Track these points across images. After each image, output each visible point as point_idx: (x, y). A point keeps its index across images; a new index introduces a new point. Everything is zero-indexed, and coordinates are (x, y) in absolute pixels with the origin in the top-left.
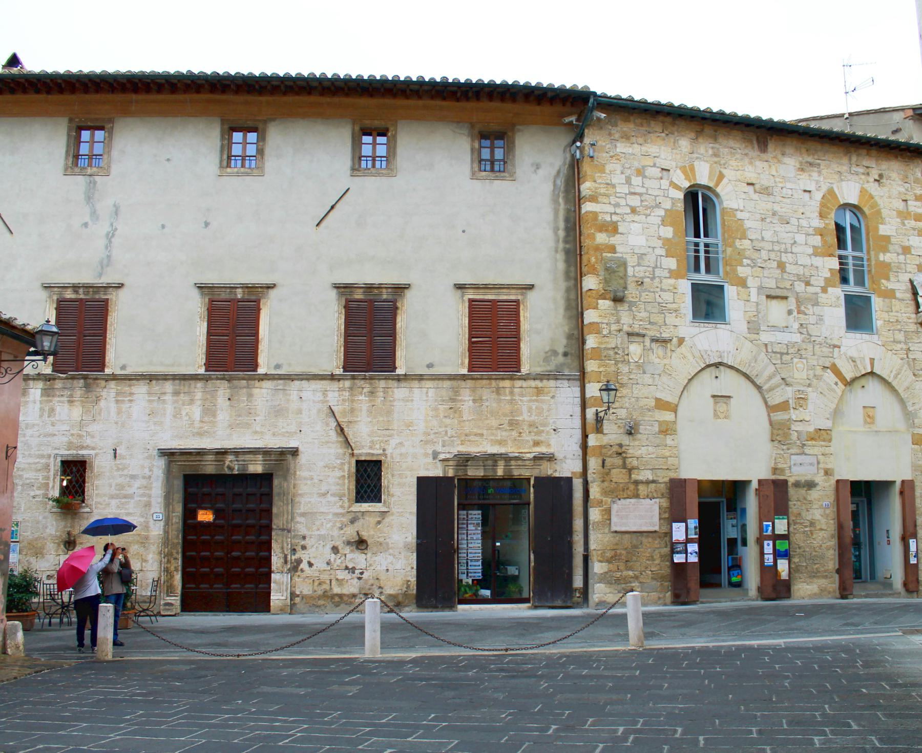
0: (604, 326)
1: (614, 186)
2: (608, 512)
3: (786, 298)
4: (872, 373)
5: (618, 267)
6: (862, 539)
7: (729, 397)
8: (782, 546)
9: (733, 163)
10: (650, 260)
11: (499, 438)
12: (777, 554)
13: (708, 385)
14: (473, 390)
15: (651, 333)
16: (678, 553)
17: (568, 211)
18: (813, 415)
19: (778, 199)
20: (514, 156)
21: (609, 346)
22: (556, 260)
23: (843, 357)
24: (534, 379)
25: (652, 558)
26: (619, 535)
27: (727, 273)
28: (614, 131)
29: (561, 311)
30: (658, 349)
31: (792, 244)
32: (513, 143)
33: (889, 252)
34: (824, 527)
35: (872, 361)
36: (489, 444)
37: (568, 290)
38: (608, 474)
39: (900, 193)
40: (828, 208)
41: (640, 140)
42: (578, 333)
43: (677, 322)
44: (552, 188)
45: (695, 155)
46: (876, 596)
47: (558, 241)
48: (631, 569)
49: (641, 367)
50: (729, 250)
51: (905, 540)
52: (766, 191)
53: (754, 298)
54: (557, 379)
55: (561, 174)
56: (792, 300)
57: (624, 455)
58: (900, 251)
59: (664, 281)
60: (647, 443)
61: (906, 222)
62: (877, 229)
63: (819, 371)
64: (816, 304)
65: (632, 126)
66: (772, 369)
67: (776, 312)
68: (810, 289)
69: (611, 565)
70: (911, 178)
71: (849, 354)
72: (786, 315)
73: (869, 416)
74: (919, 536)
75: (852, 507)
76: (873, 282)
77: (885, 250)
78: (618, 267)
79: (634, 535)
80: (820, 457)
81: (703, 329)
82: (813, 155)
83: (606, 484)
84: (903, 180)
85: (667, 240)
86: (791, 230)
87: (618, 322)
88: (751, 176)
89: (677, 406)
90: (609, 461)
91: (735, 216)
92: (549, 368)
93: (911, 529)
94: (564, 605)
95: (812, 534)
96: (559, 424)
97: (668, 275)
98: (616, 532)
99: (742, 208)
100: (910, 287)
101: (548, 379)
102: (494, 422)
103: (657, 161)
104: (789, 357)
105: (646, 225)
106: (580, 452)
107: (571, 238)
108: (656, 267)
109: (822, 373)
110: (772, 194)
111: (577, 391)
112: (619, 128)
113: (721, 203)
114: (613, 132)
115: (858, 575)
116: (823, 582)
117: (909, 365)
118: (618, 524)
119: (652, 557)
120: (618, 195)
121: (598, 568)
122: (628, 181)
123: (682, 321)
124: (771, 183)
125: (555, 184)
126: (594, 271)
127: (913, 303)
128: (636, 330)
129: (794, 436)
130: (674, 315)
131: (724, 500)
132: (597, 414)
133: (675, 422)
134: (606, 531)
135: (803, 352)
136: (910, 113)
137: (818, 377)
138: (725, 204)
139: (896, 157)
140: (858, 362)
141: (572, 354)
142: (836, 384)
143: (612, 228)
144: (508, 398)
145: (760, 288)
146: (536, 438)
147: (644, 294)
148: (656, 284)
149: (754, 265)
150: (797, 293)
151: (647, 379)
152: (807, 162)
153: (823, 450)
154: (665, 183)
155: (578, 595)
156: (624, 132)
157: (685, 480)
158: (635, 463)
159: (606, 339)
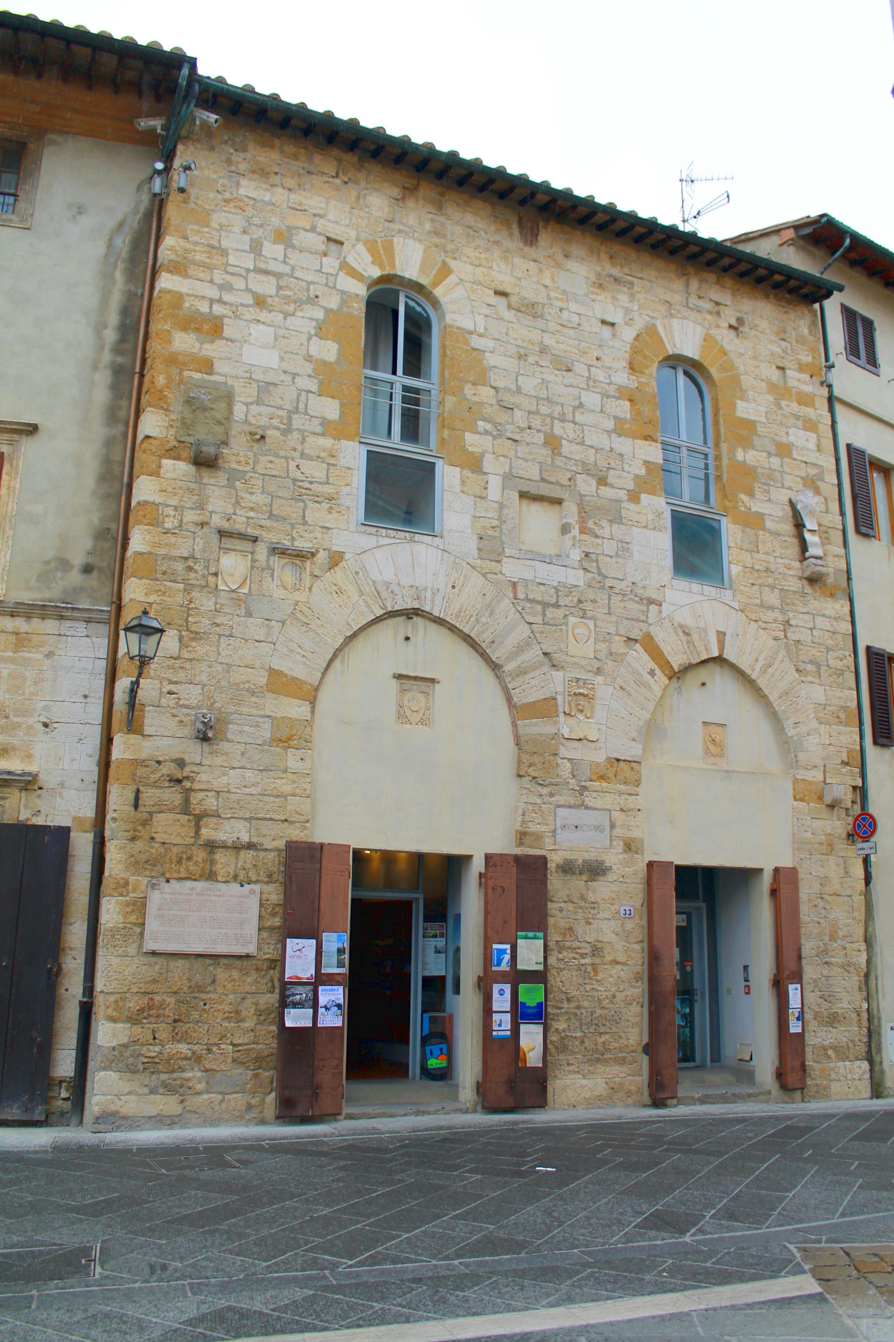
1: (224, 253)
2: (140, 906)
3: (559, 502)
4: (720, 660)
5: (216, 400)
6: (697, 984)
7: (433, 681)
8: (531, 995)
9: (469, 251)
12: (522, 1014)
13: (387, 651)
16: (295, 1005)
17: (130, 297)
18: (603, 729)
19: (552, 326)
21: (176, 553)
23: (667, 623)
25: (236, 1016)
26: (161, 960)
27: (442, 441)
28: (238, 157)
29: (90, 481)
30: (285, 572)
31: (575, 408)
33: (753, 448)
34: (622, 958)
35: (721, 635)
37: (109, 443)
40: (645, 357)
41: (290, 182)
43: (330, 520)
44: (103, 250)
45: (397, 226)
46: (724, 1099)
47: (101, 348)
48: (184, 1038)
49: (243, 603)
50: (450, 401)
51: (779, 985)
52: (530, 310)
53: (494, 491)
54: (62, 618)
55: (126, 229)
56: (571, 507)
58: (773, 450)
59: (311, 439)
60: (244, 762)
61: (783, 403)
62: (733, 406)
63: (619, 645)
64: (617, 519)
65: (275, 155)
66: (523, 632)
67: (538, 526)
68: (605, 491)
69: (137, 1030)
70: (792, 335)
73: (715, 741)
74: (806, 977)
75: (676, 920)
77: (747, 444)
79: (198, 964)
80: (616, 815)
82: (622, 266)
83: (140, 845)
84: (778, 334)
85: (325, 363)
86: (575, 383)
88: (505, 281)
89: (317, 689)
90: (149, 796)
91: (467, 342)
92: (47, 595)
93: (789, 965)
94: (24, 1118)
95: (595, 971)
97: (319, 429)
98: (154, 953)
99: (482, 331)
100: (790, 514)
103: (320, 223)
104: (560, 613)
105: (282, 332)
109: (623, 649)
110: (542, 317)
112: (248, 156)
115: (687, 1054)
116: (617, 1073)
117: (788, 651)
119: (238, 1012)
120: (229, 269)
121: (107, 1034)
122: (256, 248)
123: (342, 522)
124: (541, 298)
125: (110, 245)
126: (162, 403)
127: (795, 541)
131: (420, 896)
133: (309, 723)
134: (132, 950)
135: (588, 606)
137: (617, 658)
138: (449, 318)
139: (767, 296)
140: (695, 637)
141: (101, 570)
142: (652, 673)
143: (213, 329)
145: (508, 478)
147: (263, 460)
148: (292, 444)
149: (498, 433)
150: (581, 496)
151: (254, 628)
152: (610, 276)
153: (622, 800)
154: (331, 263)
155: (64, 1094)
157: (322, 845)
158: (211, 802)
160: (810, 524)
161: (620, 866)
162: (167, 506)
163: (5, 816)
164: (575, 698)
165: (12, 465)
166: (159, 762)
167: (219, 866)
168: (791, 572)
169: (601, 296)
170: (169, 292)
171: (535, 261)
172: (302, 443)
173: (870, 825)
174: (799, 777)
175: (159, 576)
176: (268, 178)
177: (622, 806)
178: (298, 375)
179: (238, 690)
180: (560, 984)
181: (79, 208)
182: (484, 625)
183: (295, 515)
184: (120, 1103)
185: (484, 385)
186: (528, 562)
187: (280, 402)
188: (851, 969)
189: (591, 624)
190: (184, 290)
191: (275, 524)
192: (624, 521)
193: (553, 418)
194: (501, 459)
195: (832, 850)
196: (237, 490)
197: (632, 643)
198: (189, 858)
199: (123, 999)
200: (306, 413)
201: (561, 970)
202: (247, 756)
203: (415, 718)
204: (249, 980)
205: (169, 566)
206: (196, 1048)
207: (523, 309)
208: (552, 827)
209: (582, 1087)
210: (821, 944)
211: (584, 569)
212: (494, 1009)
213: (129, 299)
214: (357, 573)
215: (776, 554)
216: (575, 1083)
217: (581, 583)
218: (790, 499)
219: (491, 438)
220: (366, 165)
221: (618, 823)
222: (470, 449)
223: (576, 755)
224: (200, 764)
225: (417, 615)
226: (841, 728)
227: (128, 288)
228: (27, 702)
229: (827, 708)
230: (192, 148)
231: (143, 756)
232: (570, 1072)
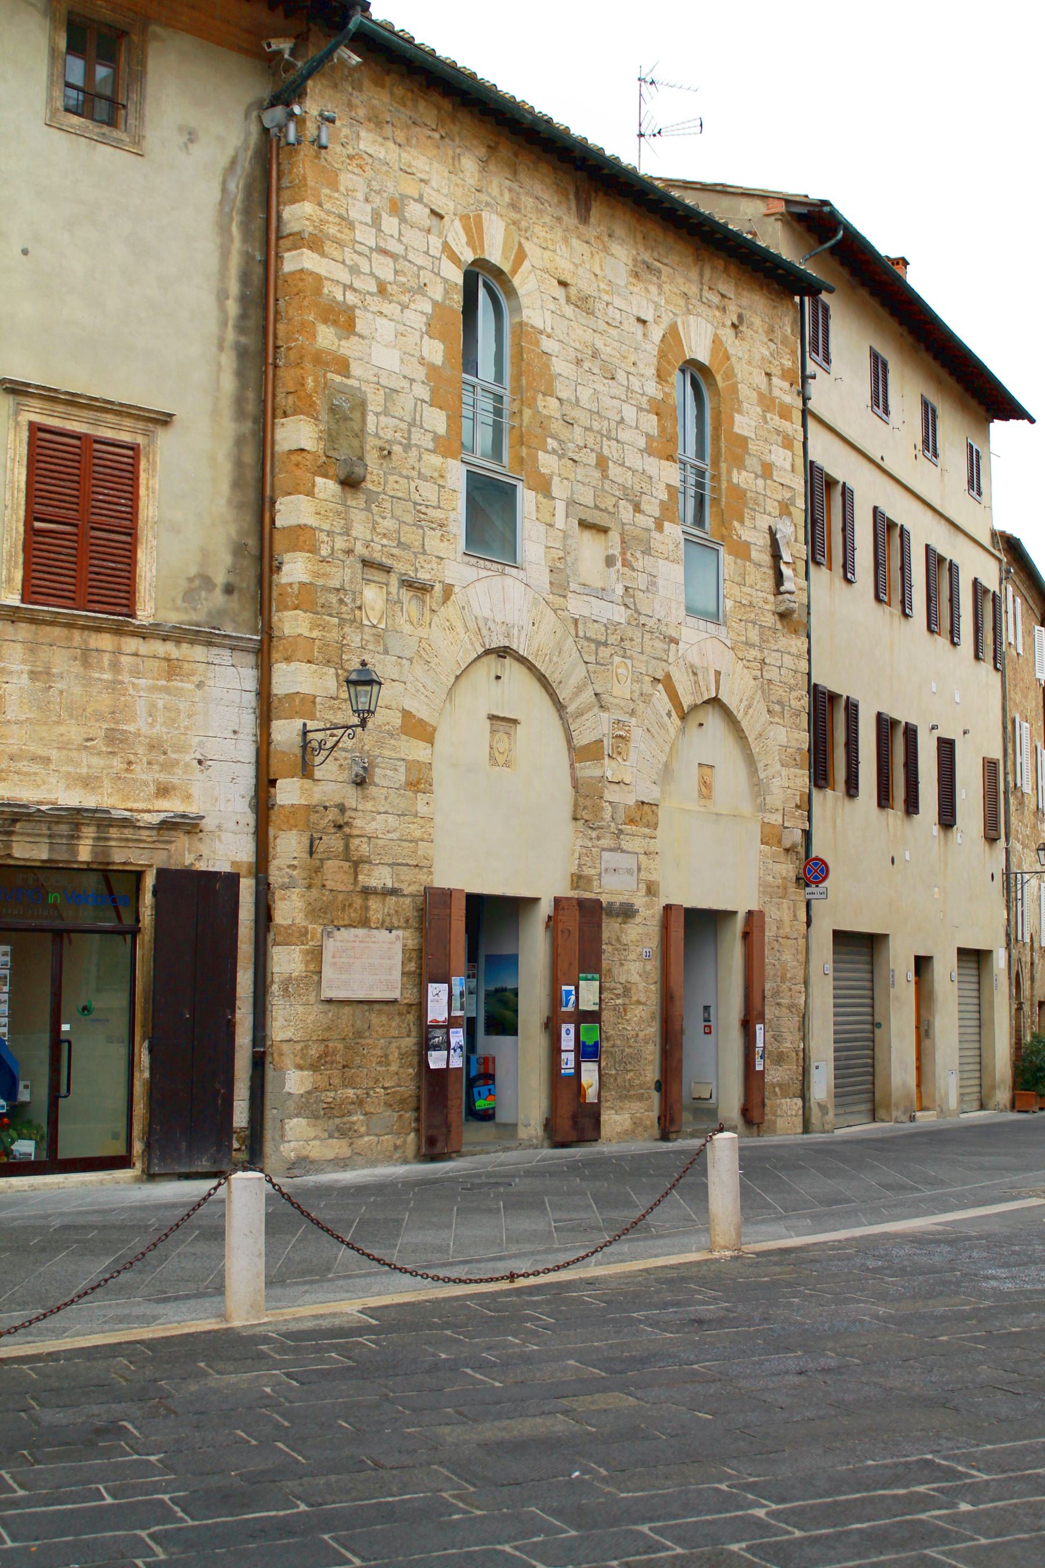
0: (323, 536)
1: (351, 226)
2: (316, 956)
3: (604, 530)
4: (715, 702)
7: (515, 722)
8: (590, 1034)
10: (404, 405)
11: (84, 770)
12: (586, 1052)
14: (32, 647)
18: (631, 776)
20: (142, 96)
22: (219, 367)
24: (165, 639)
25: (384, 1060)
32: (143, 63)
34: (643, 1000)
36: (62, 785)
38: (318, 870)
39: (763, 358)
41: (401, 137)
42: (260, 550)
44: (219, 196)
45: (484, 197)
47: (224, 324)
48: (349, 1083)
52: (584, 304)
53: (560, 522)
54: (210, 644)
55: (239, 169)
57: (347, 830)
58: (759, 470)
61: (769, 416)
63: (647, 688)
72: (602, 564)
76: (723, 523)
77: (741, 466)
78: (352, 409)
80: (642, 857)
81: (484, 573)
83: (315, 892)
84: (767, 333)
87: (347, 532)
88: (565, 267)
91: (537, 343)
92: (195, 617)
95: (625, 1010)
96: (212, 749)
97: (431, 446)
98: (330, 1001)
101: (192, 643)
102: (74, 732)
103: (427, 190)
104: (608, 651)
106: (250, 818)
107: (251, 323)
108: (412, 424)
110: (593, 314)
111: (248, 677)
113: (518, 309)
114: (356, 101)
117: (763, 692)
118: (337, 984)
120: (358, 247)
121: (294, 1081)
122: (376, 221)
125: (224, 190)
126: (307, 408)
128: (378, 557)
130: (438, 533)
132: (305, 733)
135: (627, 644)
136: (781, 208)
142: (669, 715)
143: (344, 320)
144: (107, 676)
145: (571, 503)
146: (163, 777)
150: (623, 524)
152: (644, 262)
156: (373, 107)
159: (327, 568)
160: (786, 557)
163: (172, 861)
165: (148, 461)
166: (326, 808)
167: (371, 913)
168: (768, 607)
169: (638, 288)
170: (312, 273)
171: (587, 243)
172: (419, 461)
173: (822, 871)
174: (766, 820)
175: (319, 609)
176: (381, 128)
179: (381, 732)
181: (190, 133)
184: (309, 1148)
185: (552, 396)
186: (586, 598)
187: (402, 413)
188: (794, 1010)
190: (323, 272)
191: (403, 553)
192: (652, 552)
193: (602, 435)
194: (565, 481)
196: (373, 514)
197: (656, 683)
198: (350, 905)
199: (307, 1047)
200: (422, 427)
202: (389, 800)
204: (394, 1024)
205: (326, 598)
206: (359, 1092)
207: (579, 303)
209: (615, 1122)
211: (625, 605)
212: (563, 1048)
213: (247, 263)
214: (463, 608)
215: (758, 587)
217: (623, 621)
218: (770, 527)
219: (556, 458)
220: (459, 115)
221: (643, 867)
222: (543, 470)
224: (356, 810)
226: (797, 771)
227: (245, 248)
228: (183, 737)
229: (789, 750)
230: (319, 86)
231: (315, 802)
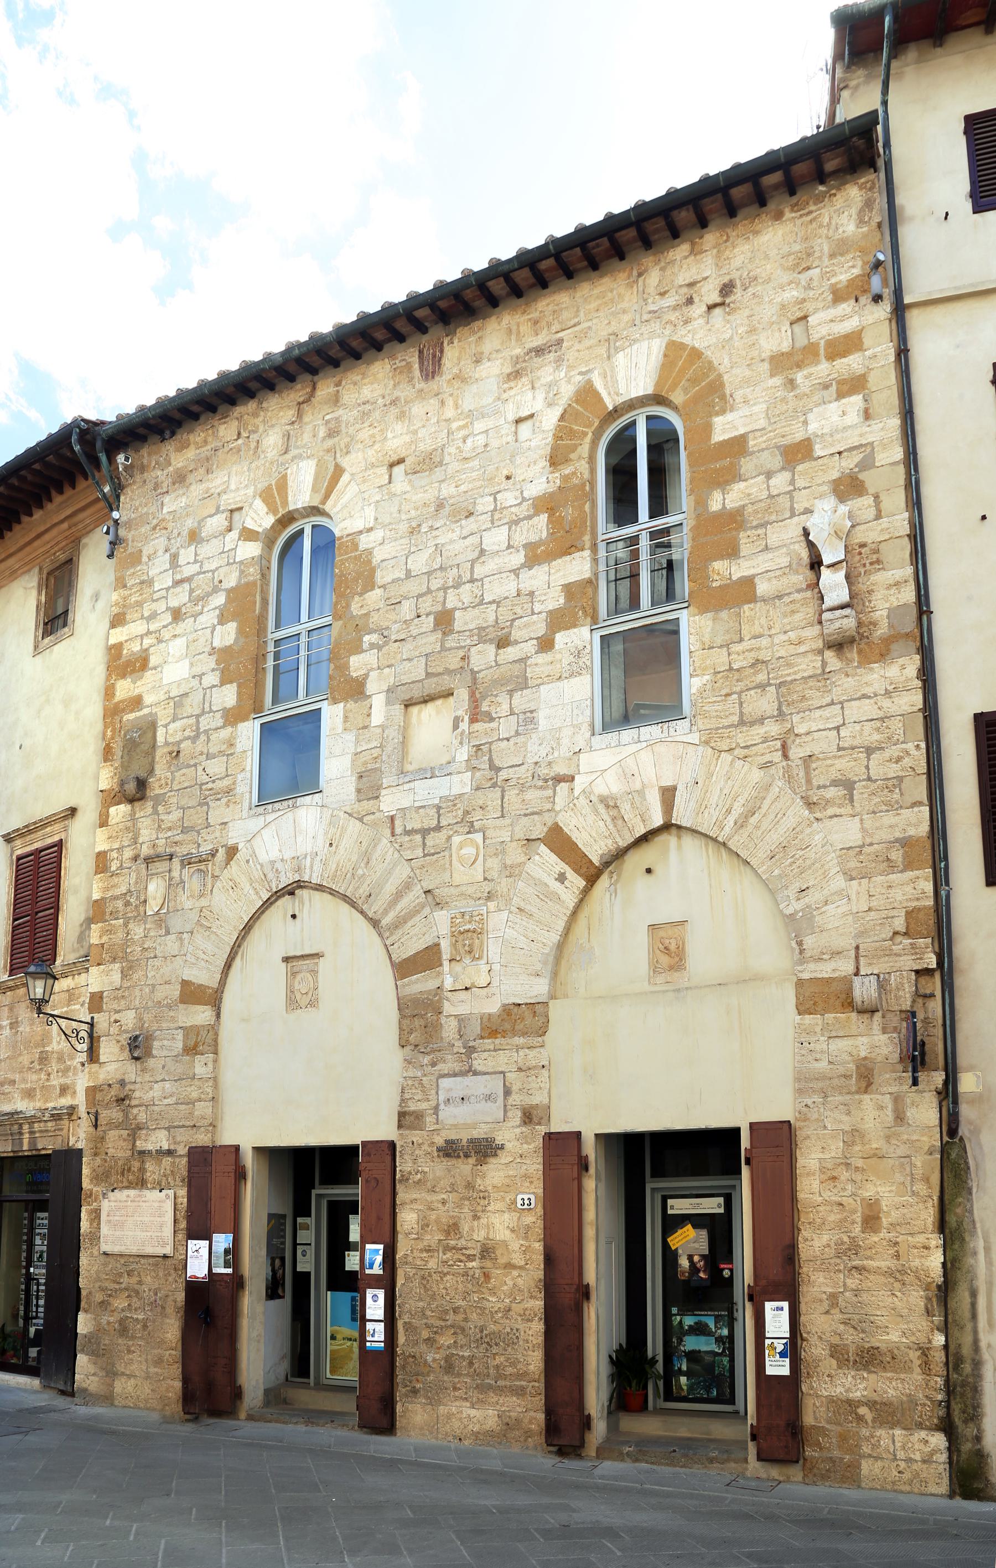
7: (317, 955)
15: (181, 850)
23: (583, 801)
34: (518, 1259)
35: (668, 795)
63: (515, 854)
66: (403, 872)
68: (511, 653)
71: (600, 789)
73: (669, 950)
81: (270, 817)
90: (105, 1115)
98: (105, 1253)
104: (443, 835)
116: (514, 1406)
117: (789, 777)
129: (449, 1029)
130: (224, 800)
135: (476, 816)
137: (512, 871)
140: (625, 808)
142: (561, 878)
148: (199, 749)
151: (171, 945)
161: (516, 1143)
162: (112, 850)
164: (461, 937)
166: (110, 1085)
167: (148, 1174)
177: (520, 1065)
178: (203, 674)
180: (444, 1291)
182: (359, 878)
183: (200, 821)
184: (88, 1382)
186: (406, 786)
189: (478, 837)
195: (869, 1084)
198: (129, 1170)
201: (445, 1275)
203: (304, 1001)
208: (433, 1103)
210: (846, 1239)
216: (462, 1412)
221: (515, 1088)
223: (462, 1010)
225: (301, 887)
231: (100, 1082)
232: (456, 1399)
